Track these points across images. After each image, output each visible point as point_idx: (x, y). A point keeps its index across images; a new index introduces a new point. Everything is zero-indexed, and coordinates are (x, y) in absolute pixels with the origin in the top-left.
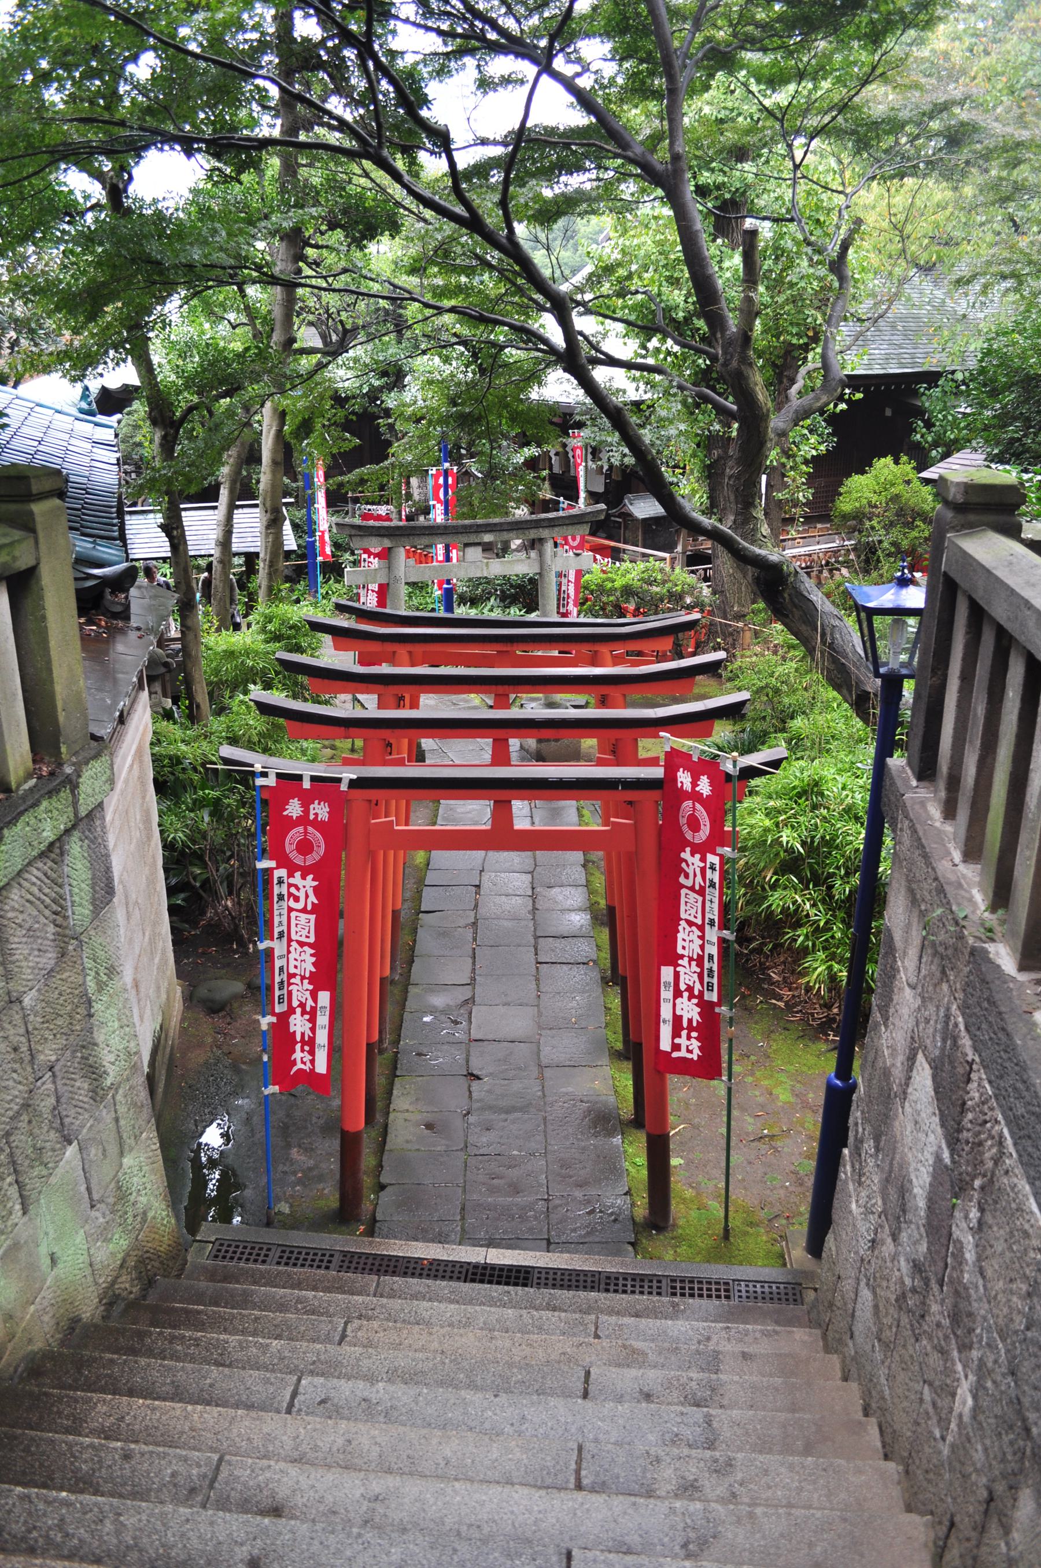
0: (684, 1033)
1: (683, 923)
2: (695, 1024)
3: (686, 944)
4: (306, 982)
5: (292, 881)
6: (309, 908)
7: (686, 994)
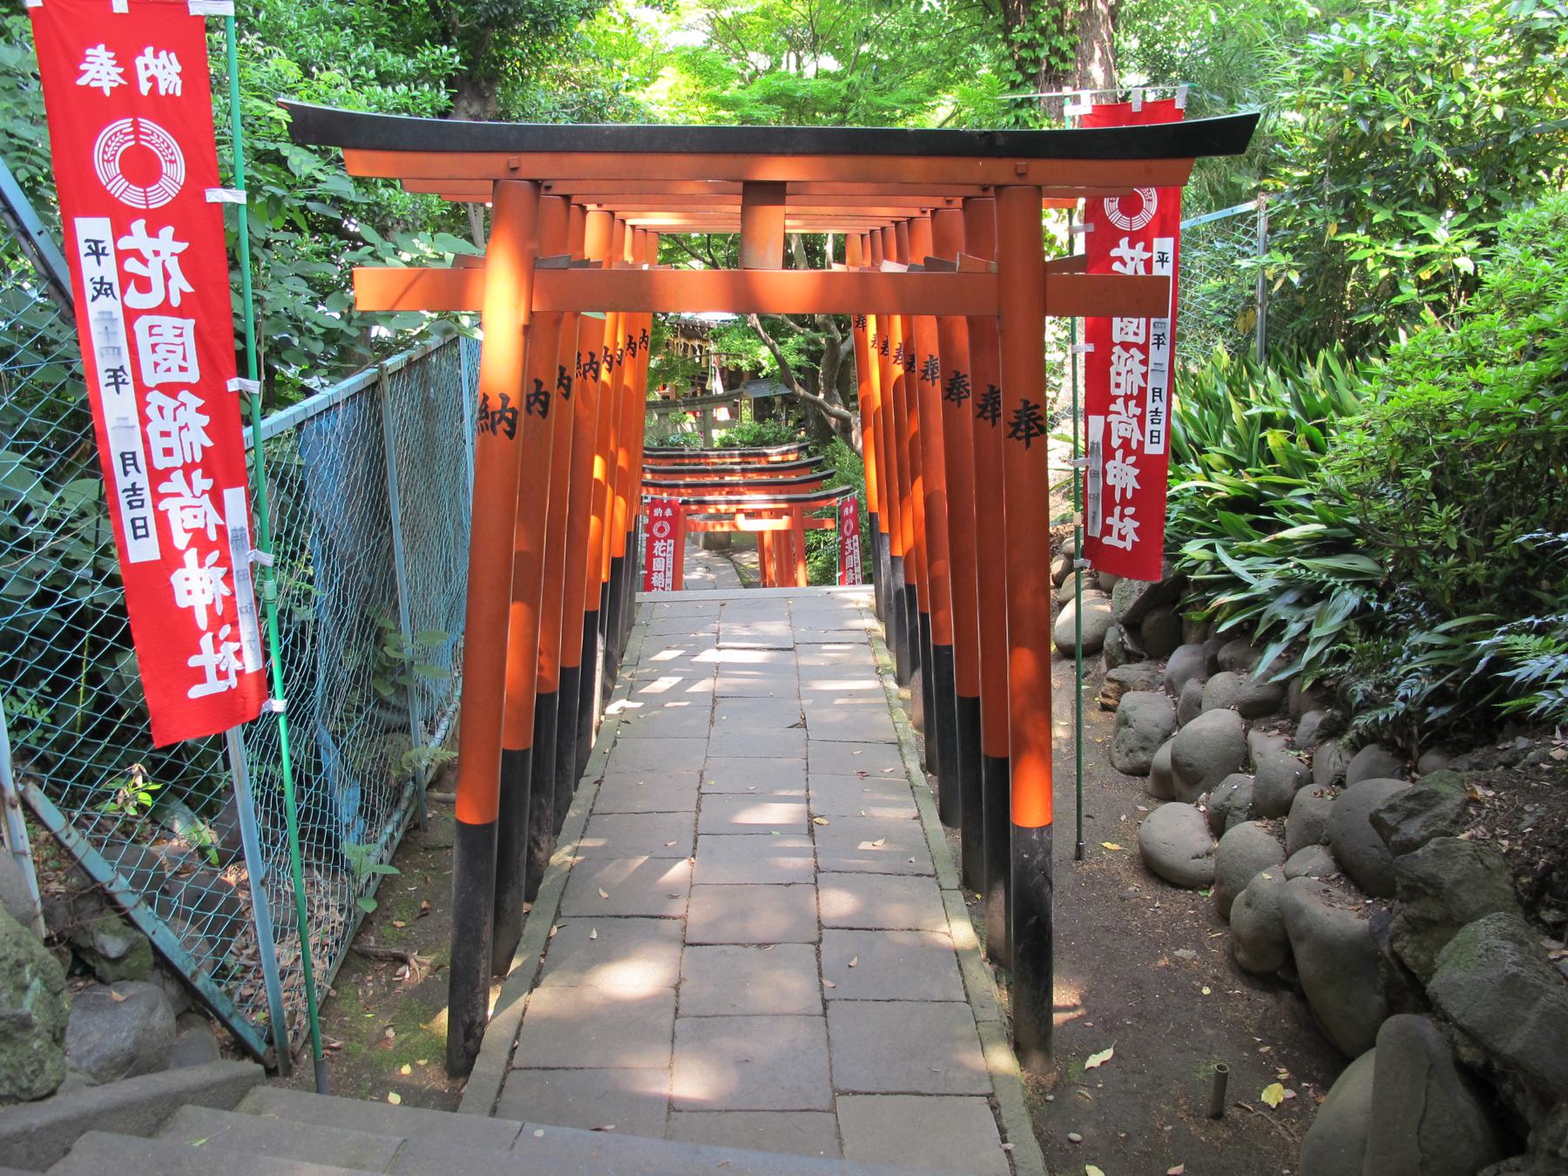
0: (1117, 510)
1: (1117, 349)
2: (1129, 495)
3: (1121, 380)
5: (125, 243)
6: (176, 301)
7: (1119, 454)
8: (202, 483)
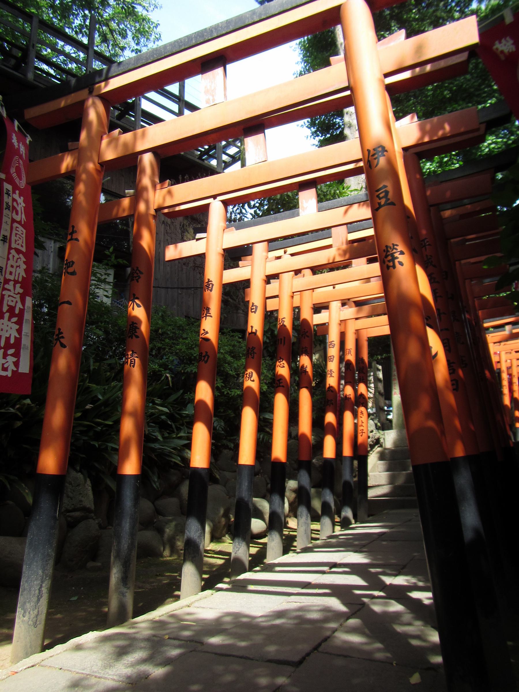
3: (13, 270)
4: (18, 286)
8: (19, 290)
